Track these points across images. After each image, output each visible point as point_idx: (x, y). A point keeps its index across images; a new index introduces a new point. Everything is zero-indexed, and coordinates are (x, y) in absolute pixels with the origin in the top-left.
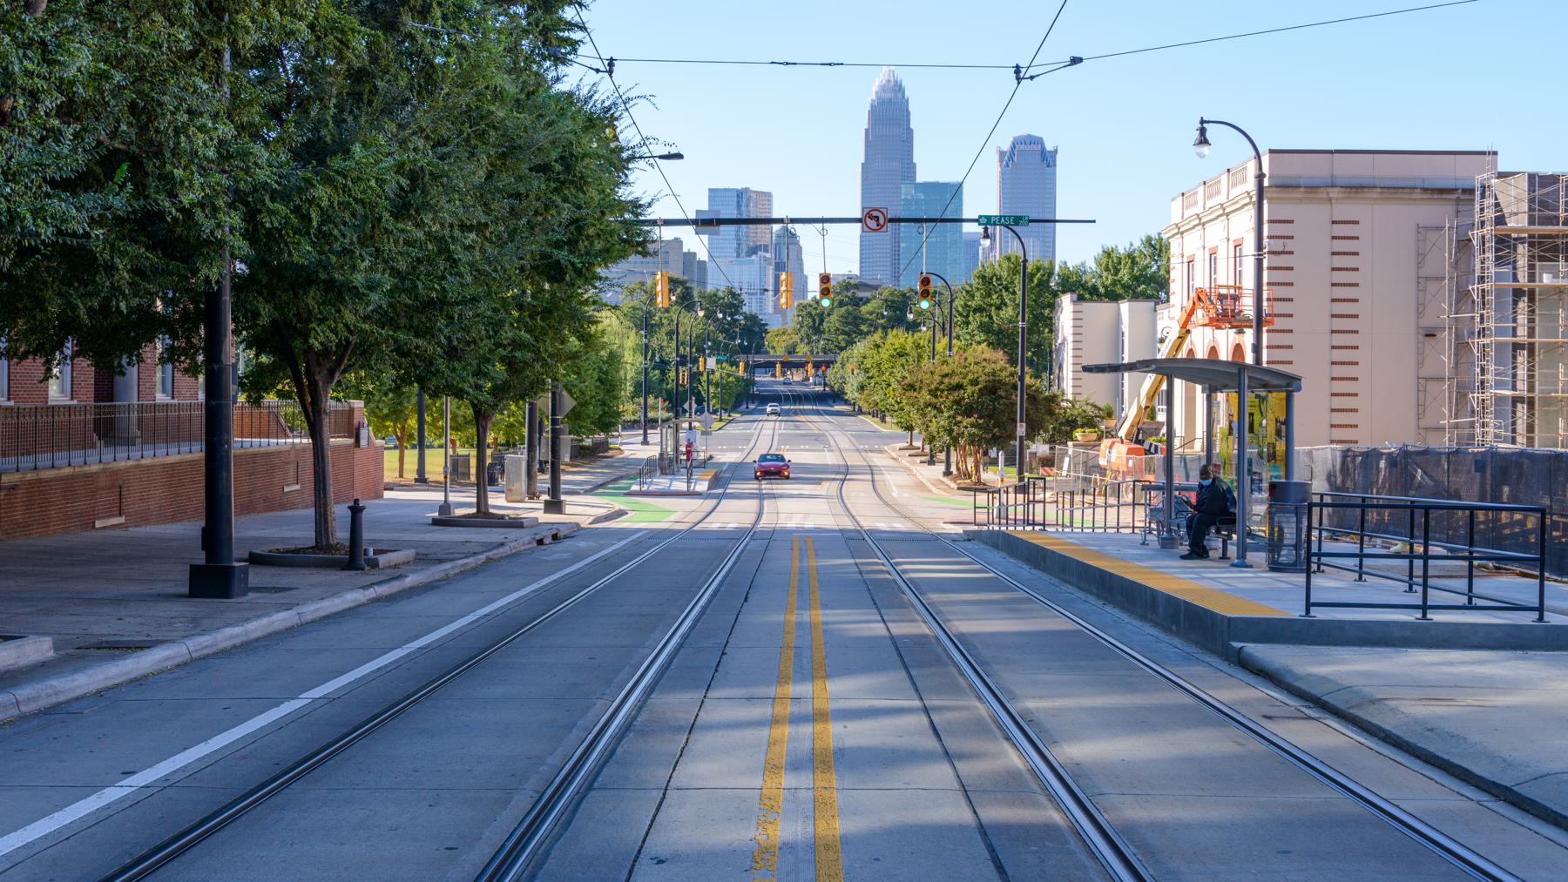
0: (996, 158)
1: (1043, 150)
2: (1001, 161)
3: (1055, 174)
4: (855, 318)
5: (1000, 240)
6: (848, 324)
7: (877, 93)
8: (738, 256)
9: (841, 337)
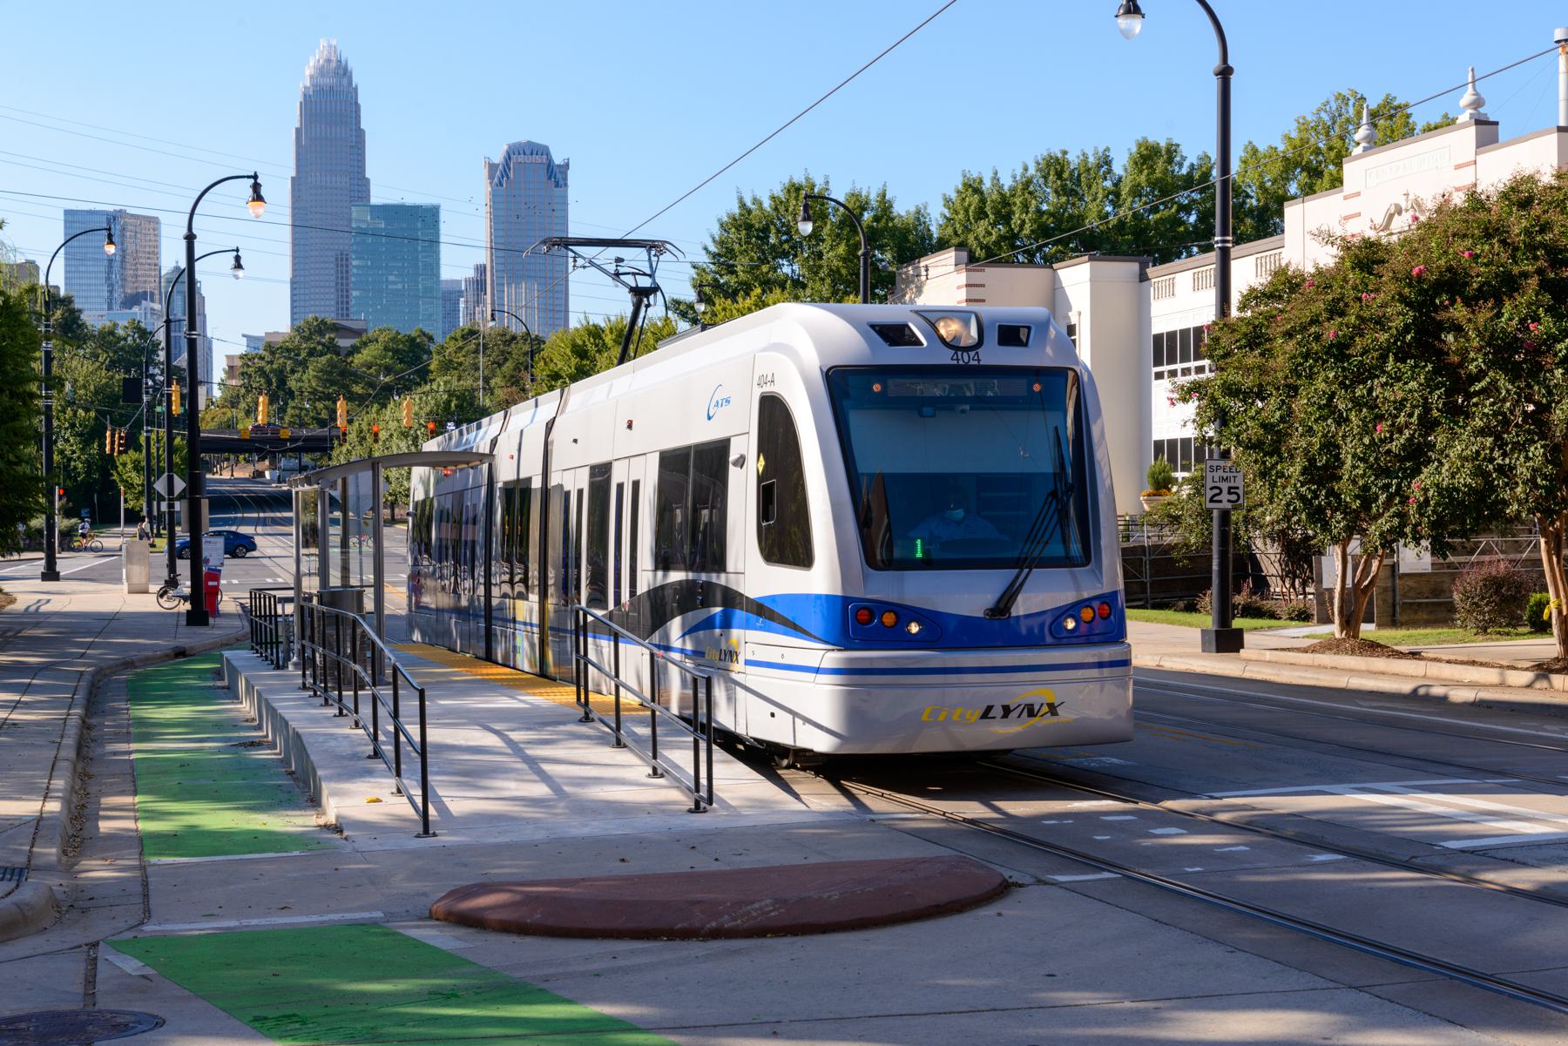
0: (485, 172)
1: (550, 165)
2: (491, 177)
3: (566, 197)
4: (343, 374)
5: (492, 289)
6: (333, 383)
7: (311, 77)
8: (110, 308)
9: (320, 405)
